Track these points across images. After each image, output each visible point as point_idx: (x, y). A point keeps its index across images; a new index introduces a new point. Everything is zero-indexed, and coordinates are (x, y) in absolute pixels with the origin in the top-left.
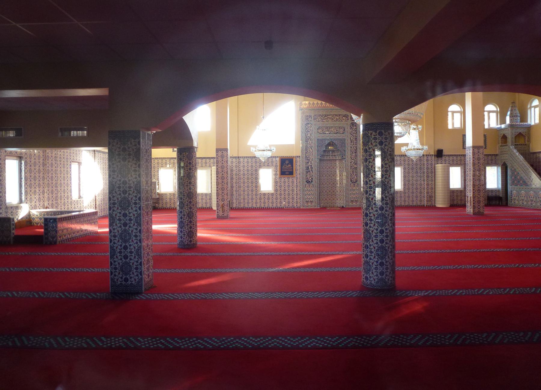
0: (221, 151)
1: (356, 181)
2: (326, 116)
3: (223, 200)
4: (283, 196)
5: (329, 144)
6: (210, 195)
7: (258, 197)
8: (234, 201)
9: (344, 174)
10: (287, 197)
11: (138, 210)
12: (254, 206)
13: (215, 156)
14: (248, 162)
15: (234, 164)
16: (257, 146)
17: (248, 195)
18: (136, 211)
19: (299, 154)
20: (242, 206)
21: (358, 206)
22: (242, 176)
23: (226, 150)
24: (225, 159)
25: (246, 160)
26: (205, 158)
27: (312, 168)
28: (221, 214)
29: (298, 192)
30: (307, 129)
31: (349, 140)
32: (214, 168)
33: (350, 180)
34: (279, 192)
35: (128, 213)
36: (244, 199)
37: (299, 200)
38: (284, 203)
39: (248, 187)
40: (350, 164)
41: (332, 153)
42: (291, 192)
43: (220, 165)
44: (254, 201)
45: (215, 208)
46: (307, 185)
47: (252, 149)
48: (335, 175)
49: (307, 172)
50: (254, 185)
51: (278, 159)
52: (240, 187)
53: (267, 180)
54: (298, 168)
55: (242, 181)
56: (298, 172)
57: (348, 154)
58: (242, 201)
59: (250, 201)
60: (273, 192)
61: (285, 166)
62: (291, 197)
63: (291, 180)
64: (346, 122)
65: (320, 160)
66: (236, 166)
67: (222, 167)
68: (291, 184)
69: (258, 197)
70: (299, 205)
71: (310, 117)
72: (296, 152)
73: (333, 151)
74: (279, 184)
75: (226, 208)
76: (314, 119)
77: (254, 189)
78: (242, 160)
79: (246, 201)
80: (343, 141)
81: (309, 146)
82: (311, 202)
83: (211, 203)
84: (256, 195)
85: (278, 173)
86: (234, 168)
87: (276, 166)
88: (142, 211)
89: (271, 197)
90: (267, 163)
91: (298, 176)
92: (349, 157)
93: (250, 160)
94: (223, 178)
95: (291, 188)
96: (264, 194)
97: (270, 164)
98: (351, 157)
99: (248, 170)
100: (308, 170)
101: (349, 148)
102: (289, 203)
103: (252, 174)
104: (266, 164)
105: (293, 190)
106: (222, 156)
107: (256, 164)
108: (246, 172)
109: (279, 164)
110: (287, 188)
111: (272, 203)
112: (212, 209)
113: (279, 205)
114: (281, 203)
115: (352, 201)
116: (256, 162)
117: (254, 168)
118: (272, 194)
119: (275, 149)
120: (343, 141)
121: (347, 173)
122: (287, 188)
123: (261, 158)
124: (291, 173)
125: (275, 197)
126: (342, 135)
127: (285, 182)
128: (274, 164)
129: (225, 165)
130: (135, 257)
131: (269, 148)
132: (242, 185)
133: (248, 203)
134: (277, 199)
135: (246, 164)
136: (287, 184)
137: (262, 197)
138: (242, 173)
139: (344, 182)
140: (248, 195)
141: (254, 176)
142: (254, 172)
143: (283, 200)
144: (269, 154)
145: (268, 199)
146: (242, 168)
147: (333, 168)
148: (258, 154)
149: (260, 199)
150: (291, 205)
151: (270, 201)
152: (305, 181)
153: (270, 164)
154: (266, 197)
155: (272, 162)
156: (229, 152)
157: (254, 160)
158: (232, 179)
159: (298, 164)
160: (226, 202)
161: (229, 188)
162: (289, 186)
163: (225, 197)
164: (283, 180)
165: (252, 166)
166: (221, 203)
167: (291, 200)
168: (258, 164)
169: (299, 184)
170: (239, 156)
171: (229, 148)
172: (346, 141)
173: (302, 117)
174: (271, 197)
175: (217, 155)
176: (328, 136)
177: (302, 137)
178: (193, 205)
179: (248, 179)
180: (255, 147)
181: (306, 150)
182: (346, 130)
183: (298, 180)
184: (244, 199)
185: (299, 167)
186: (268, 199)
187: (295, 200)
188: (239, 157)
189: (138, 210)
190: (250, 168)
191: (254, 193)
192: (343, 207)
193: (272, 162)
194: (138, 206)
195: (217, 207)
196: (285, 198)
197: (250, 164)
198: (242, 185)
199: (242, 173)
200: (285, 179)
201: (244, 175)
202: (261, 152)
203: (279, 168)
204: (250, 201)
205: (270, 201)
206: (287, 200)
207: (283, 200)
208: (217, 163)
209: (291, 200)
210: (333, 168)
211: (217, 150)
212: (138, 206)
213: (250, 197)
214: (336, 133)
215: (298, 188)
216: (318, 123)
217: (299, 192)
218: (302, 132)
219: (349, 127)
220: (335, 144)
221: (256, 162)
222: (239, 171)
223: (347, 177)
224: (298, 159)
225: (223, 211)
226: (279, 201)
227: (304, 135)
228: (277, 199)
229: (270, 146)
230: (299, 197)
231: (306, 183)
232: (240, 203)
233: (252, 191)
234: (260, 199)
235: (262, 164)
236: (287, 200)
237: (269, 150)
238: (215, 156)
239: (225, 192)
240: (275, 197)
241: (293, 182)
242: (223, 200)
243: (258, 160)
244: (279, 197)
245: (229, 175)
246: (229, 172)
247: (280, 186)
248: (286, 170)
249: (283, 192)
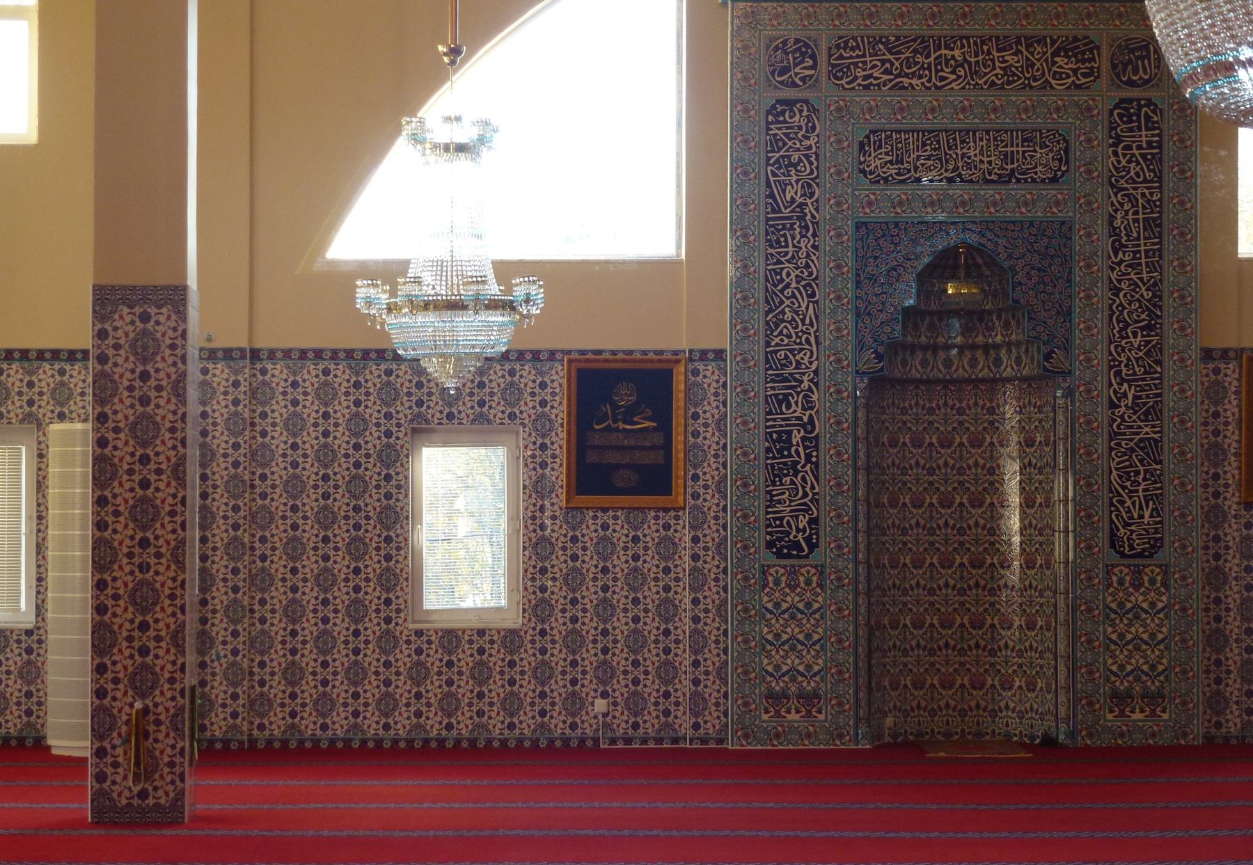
0: (138, 305)
1: (1156, 545)
2: (924, 44)
3: (143, 681)
4: (589, 656)
5: (946, 264)
6: (32, 640)
7: (403, 657)
8: (219, 689)
9: (1063, 486)
10: (620, 658)
11: (179, 531)
12: (372, 725)
13: (84, 339)
14: (326, 393)
15: (220, 408)
16: (404, 265)
17: (324, 642)
18: (174, 531)
19: (718, 336)
20: (277, 724)
21: (1166, 739)
22: (279, 502)
23: (176, 296)
24: (163, 367)
25: (310, 374)
26: (56, 354)
27: (812, 442)
28: (124, 787)
29: (713, 628)
30: (776, 144)
31: (1101, 228)
32: (71, 438)
33: (1102, 539)
34: (558, 625)
35: (151, 537)
36: (293, 674)
37: (711, 688)
38: (601, 705)
39: (325, 580)
40: (1102, 414)
41: (966, 331)
42: (651, 626)
43: (124, 409)
44: (372, 689)
45: (68, 735)
46: (778, 570)
47: (363, 291)
48: (987, 496)
49: (775, 476)
50: (372, 564)
51: (558, 376)
52: (259, 581)
53: (465, 526)
54: (710, 439)
55: (278, 533)
56: (710, 472)
57: (1091, 335)
58: (277, 688)
59: (340, 689)
60: (514, 620)
61: (605, 418)
62: (651, 656)
63: (651, 531)
64: (1081, 97)
65: (878, 383)
66: (235, 423)
67: (144, 430)
68: (651, 564)
69: (403, 657)
70: (711, 725)
71: (805, 50)
72: (700, 324)
73: (973, 316)
74: (559, 563)
75: (164, 743)
76: (837, 72)
77: (372, 595)
78: (278, 373)
79: (309, 689)
80: (1051, 242)
81: (790, 273)
82: (810, 700)
83: (33, 702)
84: (388, 641)
85: (559, 474)
86: (220, 440)
87: (542, 425)
88: (188, 533)
89: (496, 657)
90: (467, 410)
91: (710, 501)
92: (1100, 355)
93: (342, 375)
94: (144, 512)
95: (651, 594)
96: (450, 638)
97: (497, 409)
98: (1114, 365)
99: (326, 455)
100: (783, 454)
101: (1101, 293)
102: (635, 703)
103: (357, 485)
104: (466, 408)
105: (667, 610)
106: (144, 348)
107: (379, 402)
108: (310, 471)
109: (560, 410)
110: (620, 595)
111: (511, 705)
112: (40, 747)
113: (558, 724)
114: (575, 703)
115: (1121, 700)
116: (389, 393)
117: (373, 440)
118: (511, 638)
119: (537, 292)
120: (1051, 242)
121: (1085, 484)
122: (620, 595)
123: (432, 366)
124: (656, 480)
125: (527, 657)
126: (1050, 192)
127: (605, 547)
128: (528, 408)
129: (164, 409)
130: (375, 527)
131: (493, 289)
132: (278, 565)
133: (324, 704)
134: (543, 673)
135: (310, 408)
136: (620, 563)
137: (434, 657)
138: (279, 471)
139: (1062, 548)
140: (324, 642)
141: (372, 502)
142: (372, 471)
143: (589, 686)
144: (486, 333)
145: (481, 673)
146: (279, 440)
147: (976, 442)
148: (410, 332)
149: (419, 673)
150: (651, 723)
151: (496, 689)
152: (760, 538)
153: (497, 409)
154: (465, 658)
155: (512, 391)
156: (193, 313)
157: (373, 374)
158: (207, 515)
159: (710, 410)
160: (164, 701)
161: (192, 592)
162: (636, 577)
163: (162, 658)
164: (590, 529)
165: (357, 424)
166: (128, 706)
167: (651, 687)
168: (404, 409)
169: (711, 564)
170: (263, 343)
171: (192, 281)
172: (1078, 241)
173: (743, 49)
174: (496, 657)
175: (101, 335)
176: (937, 201)
177: (741, 204)
178: (399, 487)
179: (326, 518)
180: (390, 273)
181: (772, 302)
182: (1076, 152)
183: (711, 533)
184: (293, 674)
185: (717, 433)
186: (481, 673)
187: (684, 687)
188: (255, 354)
189: (179, 531)
190: (341, 440)
191: (372, 626)
192: (1049, 742)
193: (512, 391)
194: (178, 519)
195: (99, 733)
196: (605, 672)
197: (342, 409)
198: (278, 565)
199: (279, 471)
200: (609, 522)
201: (294, 486)
202: (430, 318)
203: (560, 440)
204: (340, 689)
205: (496, 689)
206: (620, 687)
207: (589, 686)
208: (100, 400)
209: (651, 687)
210: (976, 442)
211: (107, 299)
212: (178, 519)
213: (340, 658)
214: (1005, 179)
215: (711, 594)
216: (864, 99)
217: (711, 626)
218: (742, 171)
219: (1101, 133)
220: (992, 262)
221: (389, 393)
222: (260, 455)
223: (1084, 515)
224: (709, 372)
225: (145, 768)
226: (558, 688)
227: (757, 192)
228: (543, 673)
229: (506, 270)
230: (711, 658)
231: (771, 559)
232: (259, 704)
233: (356, 611)
234: (419, 673)
235: (435, 408)
236: (620, 687)
237: (494, 305)
238: (84, 339)
239: (163, 619)
240: (527, 657)
241: (667, 548)
242: (143, 681)
243: (403, 378)
244: (558, 656)
245: (194, 494)
246: (193, 471)
247: (573, 579)
248: (613, 458)
249: (590, 625)
